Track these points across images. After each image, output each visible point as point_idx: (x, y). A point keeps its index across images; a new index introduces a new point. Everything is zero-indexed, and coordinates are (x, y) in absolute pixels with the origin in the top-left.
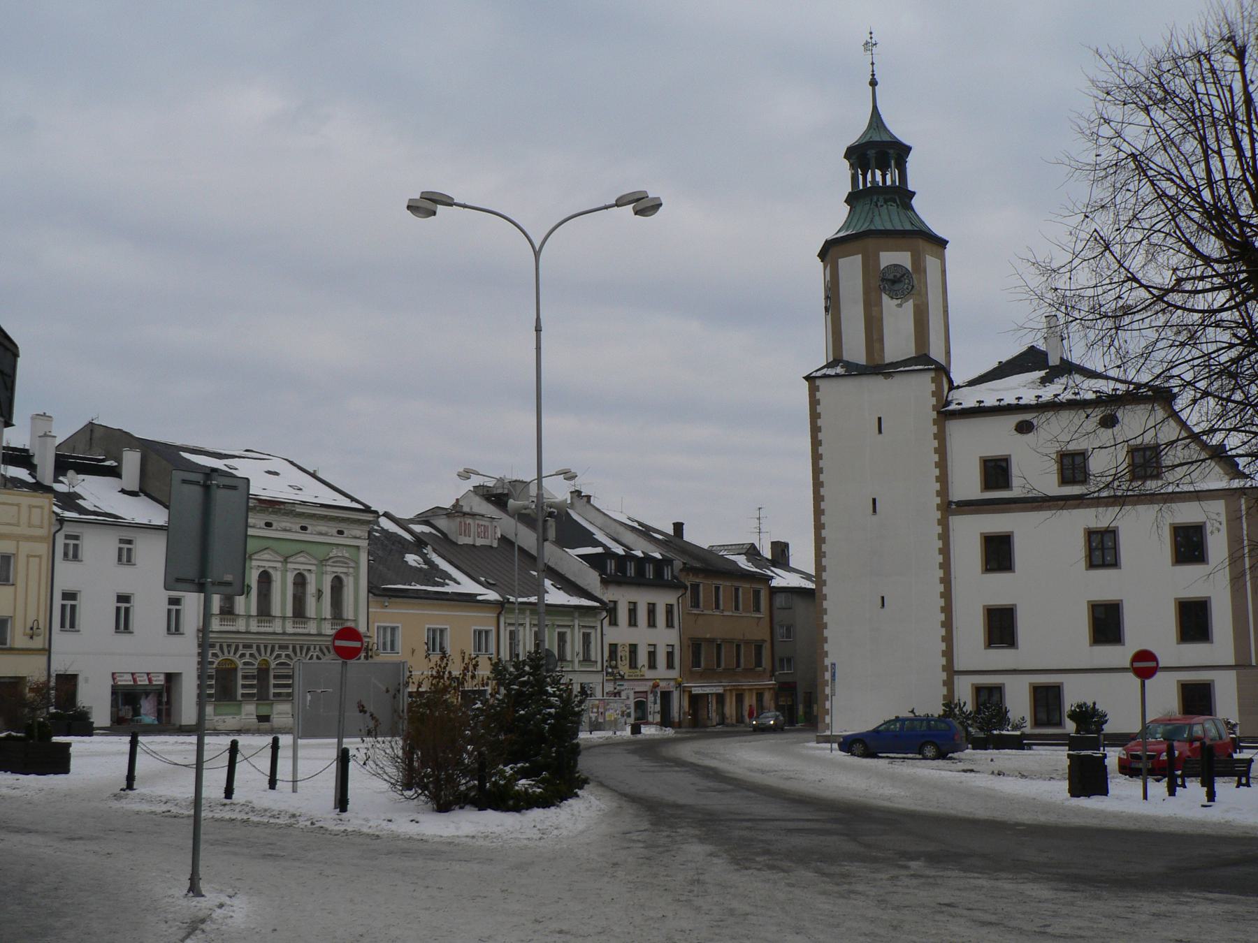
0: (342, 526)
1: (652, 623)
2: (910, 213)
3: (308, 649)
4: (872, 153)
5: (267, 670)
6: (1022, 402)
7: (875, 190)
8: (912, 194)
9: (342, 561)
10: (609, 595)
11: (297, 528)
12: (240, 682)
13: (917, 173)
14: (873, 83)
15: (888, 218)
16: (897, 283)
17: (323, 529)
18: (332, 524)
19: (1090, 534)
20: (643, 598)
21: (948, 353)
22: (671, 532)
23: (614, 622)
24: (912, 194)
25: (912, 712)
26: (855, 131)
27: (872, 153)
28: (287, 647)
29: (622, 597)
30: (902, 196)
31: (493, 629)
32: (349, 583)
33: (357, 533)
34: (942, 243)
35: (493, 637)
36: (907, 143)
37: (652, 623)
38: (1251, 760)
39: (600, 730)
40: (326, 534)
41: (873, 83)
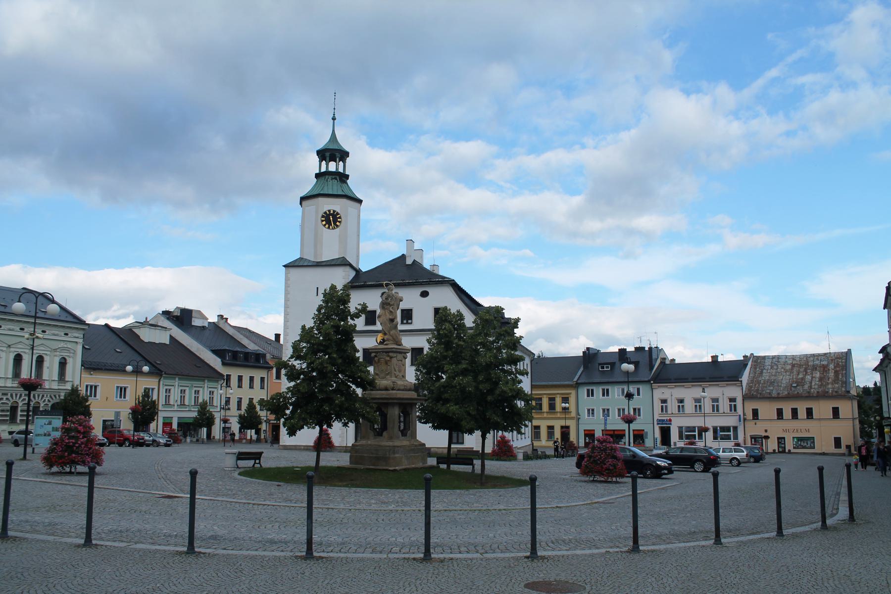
0: (67, 331)
1: (251, 386)
2: (344, 185)
3: (43, 396)
4: (327, 154)
5: (17, 407)
6: (418, 291)
7: (328, 173)
8: (347, 177)
9: (68, 350)
10: (225, 371)
11: (18, 329)
12: (19, 413)
13: (351, 167)
15: (333, 187)
16: (331, 219)
17: (12, 327)
18: (61, 329)
19: (807, 409)
20: (246, 374)
21: (358, 256)
22: (273, 339)
23: (228, 385)
24: (347, 177)
25: (766, 431)
26: (323, 142)
27: (327, 154)
28: (6, 394)
29: (234, 373)
30: (343, 177)
31: (156, 388)
32: (70, 361)
33: (77, 335)
34: (360, 201)
35: (156, 392)
36: (347, 148)
37: (251, 386)
38: (261, 453)
39: (568, 434)
40: (13, 330)
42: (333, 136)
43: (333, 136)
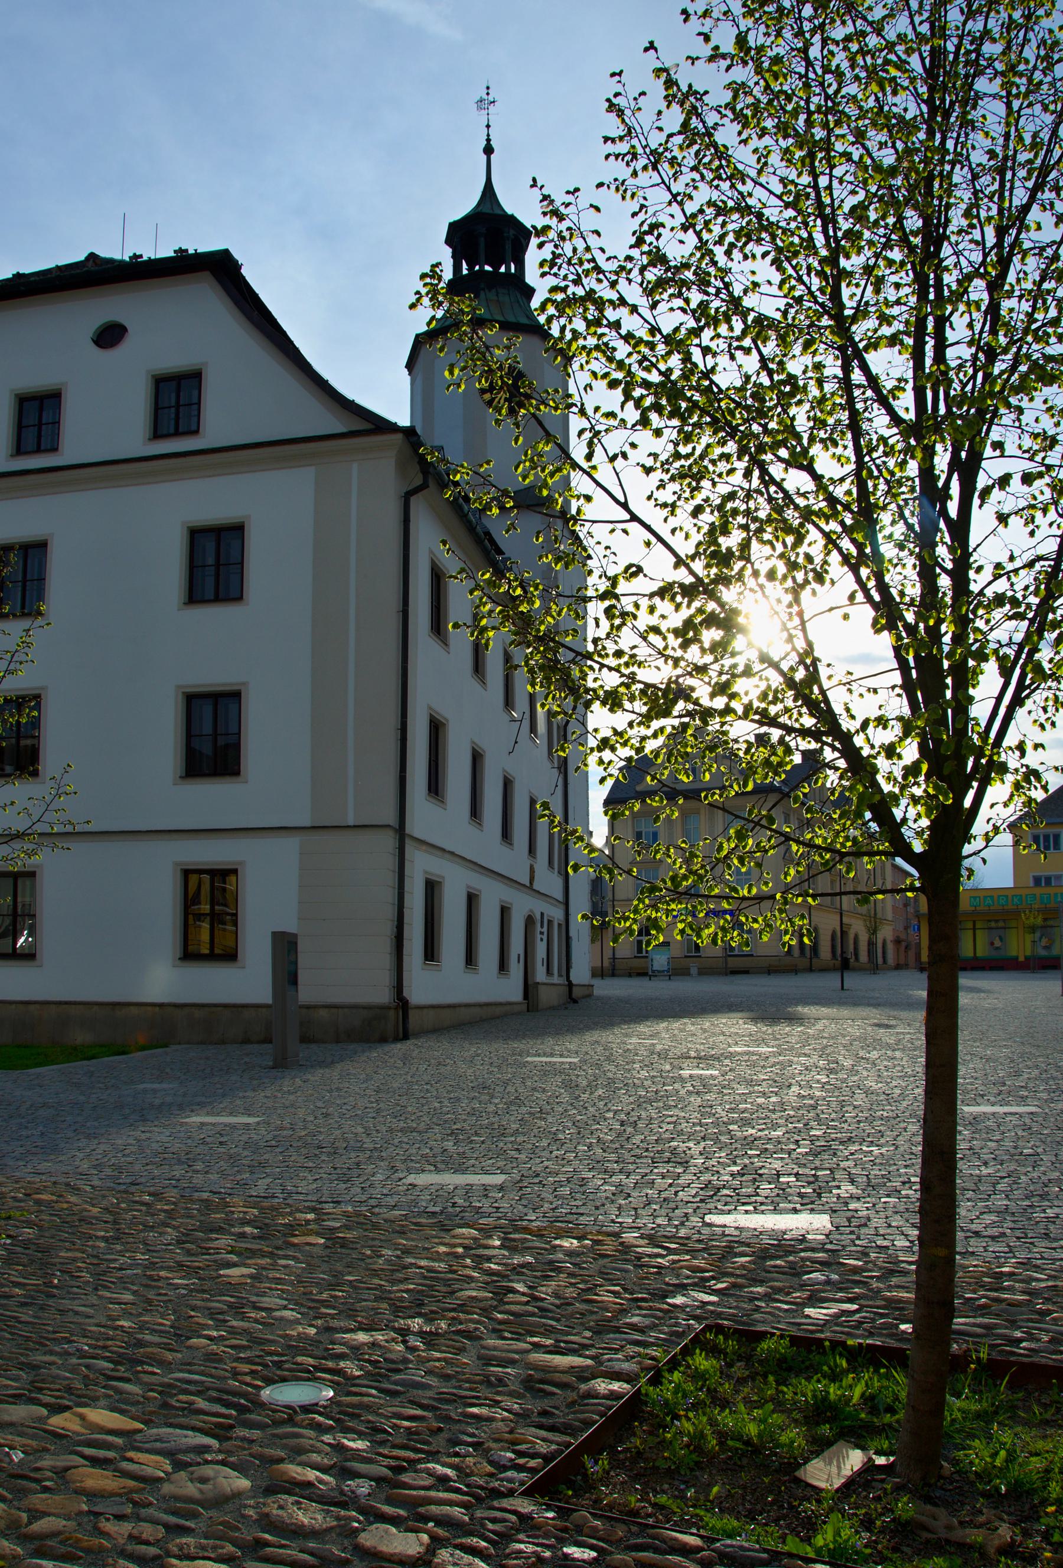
14: (488, 150)
26: (464, 203)
41: (488, 150)
42: (489, 191)
43: (489, 191)
